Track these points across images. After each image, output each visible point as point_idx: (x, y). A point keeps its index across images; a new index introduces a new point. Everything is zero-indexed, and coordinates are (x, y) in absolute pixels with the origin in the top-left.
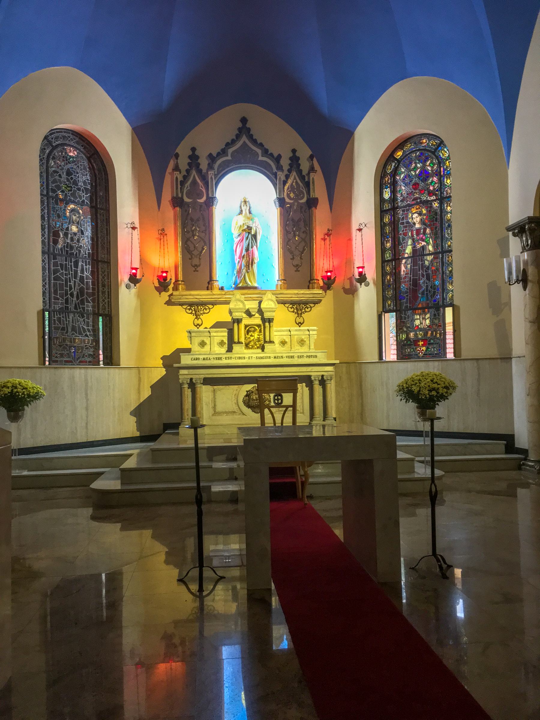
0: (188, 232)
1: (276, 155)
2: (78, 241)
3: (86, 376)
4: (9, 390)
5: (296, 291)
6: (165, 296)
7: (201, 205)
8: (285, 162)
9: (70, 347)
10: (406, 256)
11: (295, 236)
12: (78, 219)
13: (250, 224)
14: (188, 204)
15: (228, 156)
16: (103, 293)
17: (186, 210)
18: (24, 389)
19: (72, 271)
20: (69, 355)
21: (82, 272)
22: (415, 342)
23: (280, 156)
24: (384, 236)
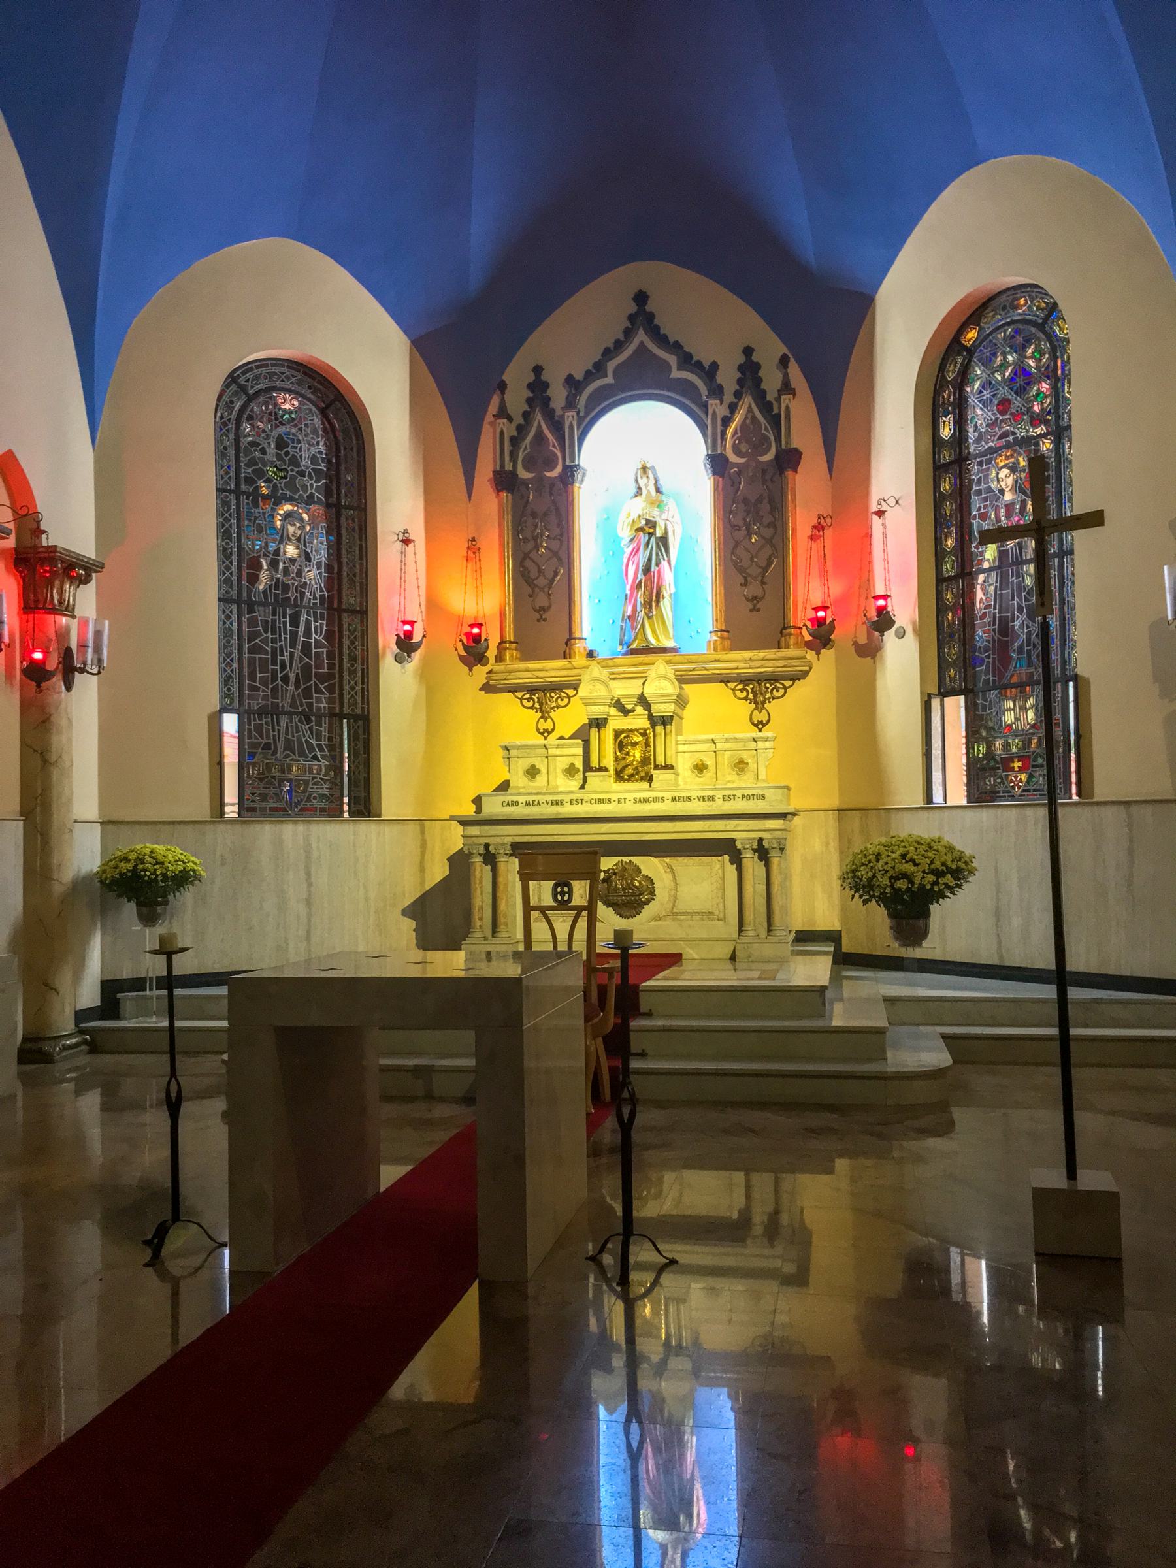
0: (525, 540)
1: (706, 364)
2: (300, 574)
3: (307, 838)
4: (130, 866)
5: (747, 654)
6: (481, 672)
7: (552, 483)
8: (728, 377)
9: (281, 781)
10: (986, 565)
11: (749, 535)
12: (299, 532)
13: (655, 515)
14: (525, 483)
15: (606, 376)
16: (352, 672)
17: (523, 496)
18: (157, 863)
19: (285, 633)
20: (278, 797)
21: (308, 633)
22: (1006, 762)
23: (715, 366)
24: (941, 524)
